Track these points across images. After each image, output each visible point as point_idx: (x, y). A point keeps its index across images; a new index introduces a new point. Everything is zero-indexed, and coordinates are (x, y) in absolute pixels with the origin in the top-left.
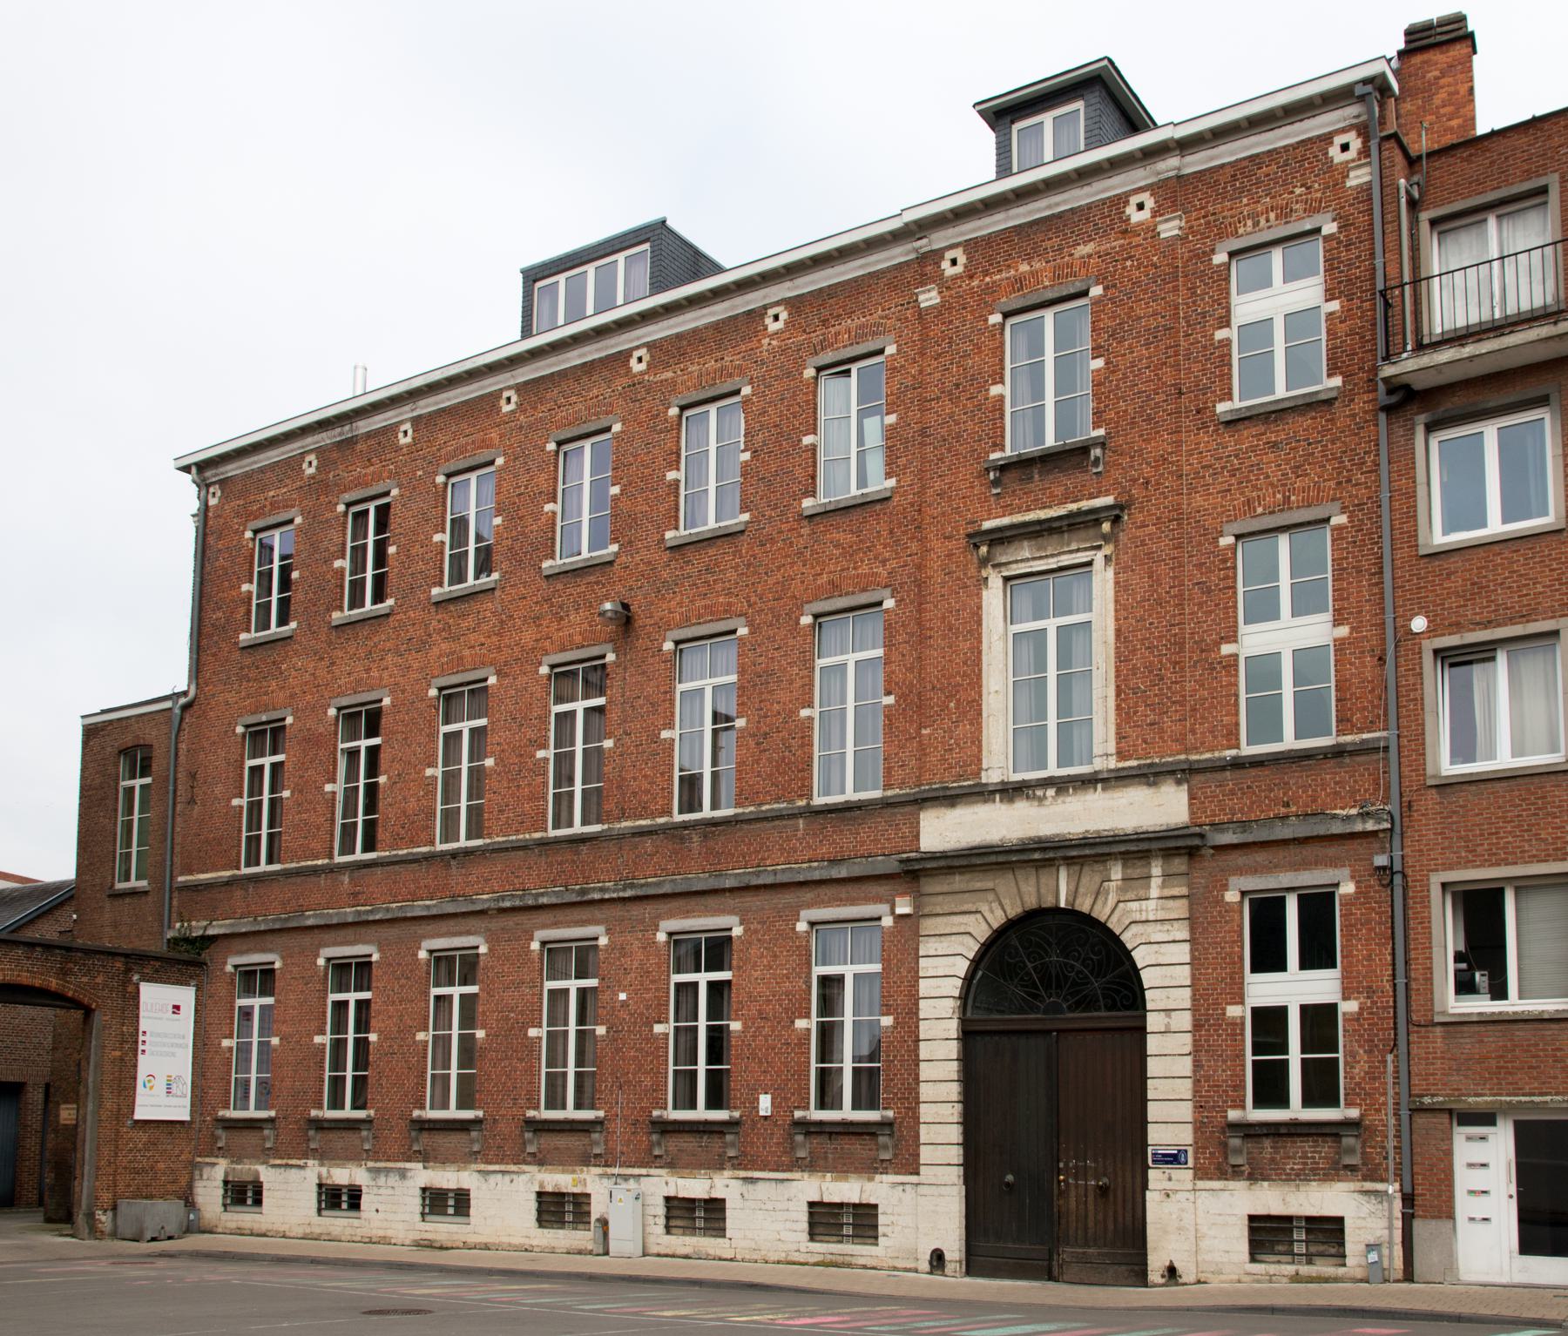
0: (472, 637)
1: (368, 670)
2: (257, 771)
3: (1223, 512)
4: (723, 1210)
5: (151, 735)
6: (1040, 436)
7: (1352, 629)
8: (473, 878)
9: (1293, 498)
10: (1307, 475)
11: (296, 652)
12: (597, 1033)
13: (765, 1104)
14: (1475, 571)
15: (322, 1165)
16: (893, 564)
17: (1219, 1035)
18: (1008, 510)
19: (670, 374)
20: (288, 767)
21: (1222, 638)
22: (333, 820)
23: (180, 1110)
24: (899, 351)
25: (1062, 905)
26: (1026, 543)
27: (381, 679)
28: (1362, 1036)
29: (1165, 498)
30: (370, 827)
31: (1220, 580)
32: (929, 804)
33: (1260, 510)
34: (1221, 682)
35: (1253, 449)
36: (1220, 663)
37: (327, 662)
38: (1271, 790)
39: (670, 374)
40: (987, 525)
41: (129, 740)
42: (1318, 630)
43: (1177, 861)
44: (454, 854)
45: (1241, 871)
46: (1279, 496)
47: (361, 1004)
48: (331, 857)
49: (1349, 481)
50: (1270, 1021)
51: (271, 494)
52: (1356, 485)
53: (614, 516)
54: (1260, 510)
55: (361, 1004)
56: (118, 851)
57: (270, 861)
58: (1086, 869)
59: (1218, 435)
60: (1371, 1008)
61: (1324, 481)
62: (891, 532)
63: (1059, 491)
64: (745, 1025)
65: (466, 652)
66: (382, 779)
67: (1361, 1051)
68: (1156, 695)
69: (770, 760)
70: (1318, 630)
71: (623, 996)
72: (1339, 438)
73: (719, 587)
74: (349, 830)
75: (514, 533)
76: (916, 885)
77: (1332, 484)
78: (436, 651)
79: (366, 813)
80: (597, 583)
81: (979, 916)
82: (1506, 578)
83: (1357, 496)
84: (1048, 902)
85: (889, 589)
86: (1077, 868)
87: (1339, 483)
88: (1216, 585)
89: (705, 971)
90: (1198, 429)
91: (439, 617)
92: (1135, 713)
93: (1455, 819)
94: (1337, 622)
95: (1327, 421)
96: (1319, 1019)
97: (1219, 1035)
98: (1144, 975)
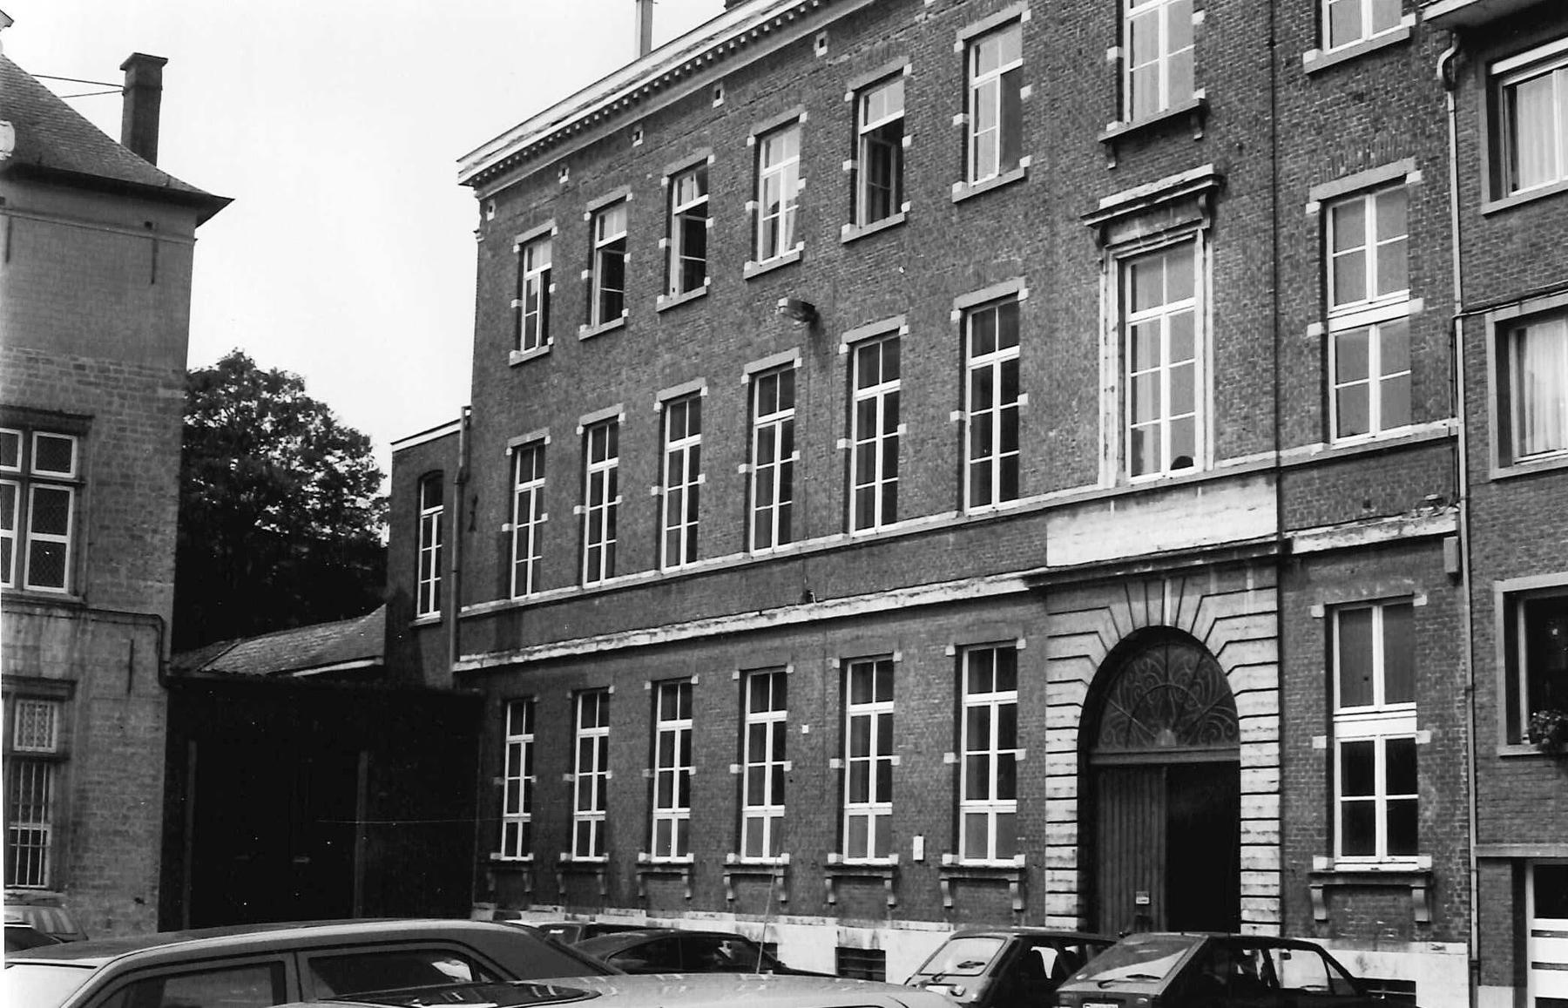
0: (690, 346)
1: (608, 385)
2: (984, 376)
3: (1310, 176)
4: (883, 965)
5: (441, 460)
6: (1155, 104)
7: (1427, 302)
8: (687, 604)
9: (1372, 156)
10: (1385, 128)
11: (555, 370)
12: (893, 763)
13: (918, 849)
14: (1533, 230)
15: (568, 911)
16: (1027, 251)
17: (1307, 771)
18: (1124, 185)
19: (845, 57)
20: (800, 426)
21: (1309, 318)
22: (581, 544)
23: (921, 858)
24: (1033, 17)
25: (1168, 624)
26: (1137, 223)
27: (618, 394)
28: (1434, 772)
29: (1258, 163)
30: (1010, 467)
31: (1308, 252)
32: (1054, 514)
33: (1343, 170)
34: (1308, 367)
35: (1336, 103)
36: (1308, 345)
37: (576, 378)
38: (1354, 489)
39: (845, 57)
40: (1105, 203)
41: (427, 466)
42: (1402, 305)
43: (1267, 573)
44: (870, 544)
45: (1327, 582)
46: (1360, 154)
47: (886, 720)
48: (579, 583)
49: (1423, 133)
50: (1359, 755)
51: (534, 205)
52: (1429, 137)
53: (1197, 52)
54: (1343, 170)
55: (886, 720)
56: (968, 462)
57: (783, 540)
58: (1188, 582)
59: (1306, 88)
60: (1442, 739)
61: (1402, 133)
62: (1026, 215)
63: (1164, 162)
64: (903, 759)
65: (684, 363)
66: (1023, 400)
67: (1433, 790)
68: (1249, 385)
69: (926, 469)
70: (1402, 305)
71: (805, 729)
72: (1414, 85)
73: (885, 284)
74: (866, 498)
75: (722, 236)
76: (1438, 552)
77: (1407, 137)
78: (659, 363)
79: (1174, 412)
80: (787, 285)
81: (1096, 636)
82: (1561, 237)
83: (1430, 150)
84: (1155, 620)
85: (1023, 278)
86: (1180, 582)
87: (1415, 135)
88: (1305, 258)
89: (774, 710)
90: (1289, 83)
91: (663, 327)
92: (1232, 405)
93: (1518, 518)
94: (1413, 295)
95: (1403, 65)
96: (1401, 751)
97: (1307, 771)
98: (1240, 701)
